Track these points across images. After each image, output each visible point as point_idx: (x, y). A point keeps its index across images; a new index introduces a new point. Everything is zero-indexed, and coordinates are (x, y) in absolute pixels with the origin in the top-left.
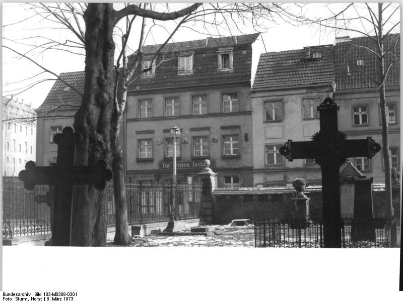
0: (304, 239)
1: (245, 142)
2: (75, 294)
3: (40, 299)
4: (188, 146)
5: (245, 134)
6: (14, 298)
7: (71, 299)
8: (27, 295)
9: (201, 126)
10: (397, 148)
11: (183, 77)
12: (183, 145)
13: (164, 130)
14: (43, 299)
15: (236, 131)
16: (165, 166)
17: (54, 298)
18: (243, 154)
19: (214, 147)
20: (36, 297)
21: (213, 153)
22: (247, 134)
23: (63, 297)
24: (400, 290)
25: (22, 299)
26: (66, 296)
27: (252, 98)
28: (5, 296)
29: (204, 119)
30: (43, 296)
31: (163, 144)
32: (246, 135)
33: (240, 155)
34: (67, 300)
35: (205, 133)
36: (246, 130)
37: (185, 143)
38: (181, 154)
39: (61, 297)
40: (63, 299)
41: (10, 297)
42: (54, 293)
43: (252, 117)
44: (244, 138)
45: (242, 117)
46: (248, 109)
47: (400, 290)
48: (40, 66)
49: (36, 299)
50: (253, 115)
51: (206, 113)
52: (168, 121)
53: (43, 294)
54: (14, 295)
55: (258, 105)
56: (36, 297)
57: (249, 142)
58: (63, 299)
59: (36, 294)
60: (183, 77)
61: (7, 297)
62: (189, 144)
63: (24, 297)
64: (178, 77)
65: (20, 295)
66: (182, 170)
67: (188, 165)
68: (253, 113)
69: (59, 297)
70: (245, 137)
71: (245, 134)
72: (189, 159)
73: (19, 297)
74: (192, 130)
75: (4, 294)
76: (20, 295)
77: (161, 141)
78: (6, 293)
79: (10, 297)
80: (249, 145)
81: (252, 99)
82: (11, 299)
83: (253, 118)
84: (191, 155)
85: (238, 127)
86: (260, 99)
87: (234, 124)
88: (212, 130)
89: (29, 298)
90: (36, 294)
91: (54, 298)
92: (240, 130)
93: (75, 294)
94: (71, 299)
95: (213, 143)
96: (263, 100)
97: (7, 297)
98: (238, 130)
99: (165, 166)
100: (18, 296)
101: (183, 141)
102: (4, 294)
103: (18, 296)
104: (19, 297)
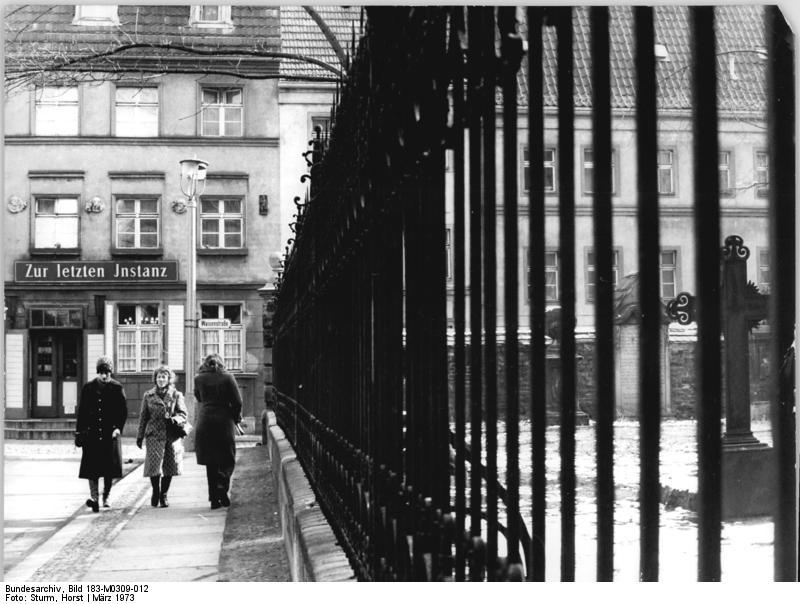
0: (48, 25)
1: (260, 218)
2: (140, 589)
3: (80, 598)
4: (101, 219)
5: (261, 197)
6: (28, 595)
7: (130, 597)
8: (54, 590)
9: (140, 169)
10: (675, 252)
11: (93, 32)
12: (86, 216)
13: (30, 173)
14: (85, 598)
15: (236, 188)
16: (32, 272)
17: (97, 596)
18: (254, 247)
19: (177, 227)
20: (72, 594)
21: (173, 241)
22: (266, 197)
23: (113, 595)
24: (542, 579)
25: (43, 599)
26: (132, 592)
27: (282, 104)
28: (10, 593)
29: (149, 148)
30: (85, 592)
31: (27, 212)
32: (263, 200)
33: (247, 250)
34: (123, 599)
35: (150, 187)
36: (264, 185)
37: (93, 210)
38: (79, 240)
39: (109, 594)
40: (114, 598)
41: (19, 594)
42: (108, 587)
43: (279, 153)
44: (257, 207)
45: (253, 152)
46: (270, 133)
47: (544, 581)
48: (30, 230)
49: (72, 598)
50: (282, 147)
51: (156, 134)
52: (43, 148)
53: (85, 589)
54: (28, 589)
55: (295, 123)
56: (72, 594)
57: (269, 216)
58: (114, 598)
59: (71, 588)
60: (93, 32)
61: (14, 594)
62: (106, 214)
63: (48, 594)
64: (76, 29)
65: (39, 590)
66: (83, 285)
67: (101, 272)
68: (281, 141)
69: (106, 594)
70: (261, 204)
71: (261, 197)
72: (105, 255)
73: (39, 594)
74: (115, 176)
75: (8, 588)
76: (39, 590)
77: (24, 203)
78: (12, 586)
79: (19, 594)
80: (270, 225)
81: (282, 108)
82: (21, 599)
83: (282, 155)
84: (108, 245)
85: (242, 177)
86: (300, 107)
87: (232, 169)
88: (169, 179)
89: (57, 595)
90: (71, 588)
91: (97, 596)
92: (248, 186)
93: (140, 589)
94: (130, 597)
95: (174, 215)
96: (309, 113)
97: (14, 594)
98: (242, 184)
99: (32, 272)
100: (35, 593)
101: (88, 206)
102: (8, 588)
103: (35, 593)
104: (39, 594)
